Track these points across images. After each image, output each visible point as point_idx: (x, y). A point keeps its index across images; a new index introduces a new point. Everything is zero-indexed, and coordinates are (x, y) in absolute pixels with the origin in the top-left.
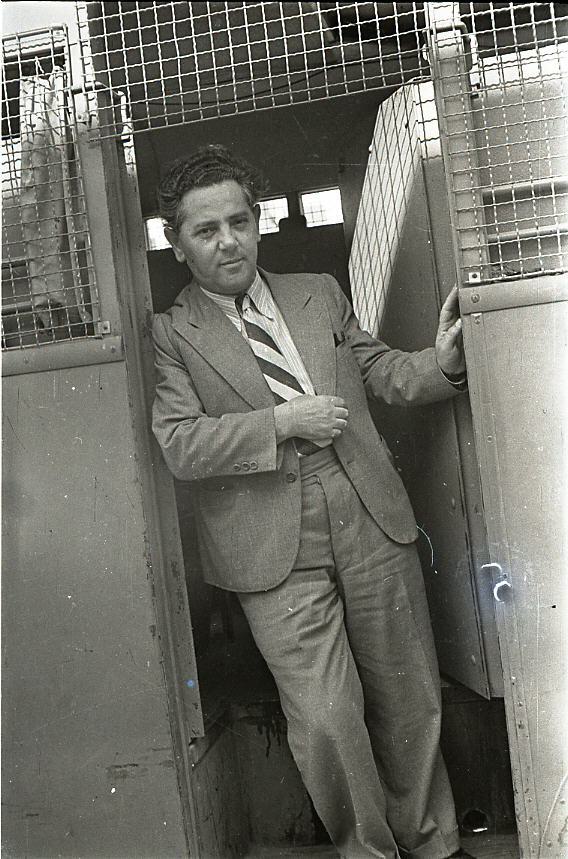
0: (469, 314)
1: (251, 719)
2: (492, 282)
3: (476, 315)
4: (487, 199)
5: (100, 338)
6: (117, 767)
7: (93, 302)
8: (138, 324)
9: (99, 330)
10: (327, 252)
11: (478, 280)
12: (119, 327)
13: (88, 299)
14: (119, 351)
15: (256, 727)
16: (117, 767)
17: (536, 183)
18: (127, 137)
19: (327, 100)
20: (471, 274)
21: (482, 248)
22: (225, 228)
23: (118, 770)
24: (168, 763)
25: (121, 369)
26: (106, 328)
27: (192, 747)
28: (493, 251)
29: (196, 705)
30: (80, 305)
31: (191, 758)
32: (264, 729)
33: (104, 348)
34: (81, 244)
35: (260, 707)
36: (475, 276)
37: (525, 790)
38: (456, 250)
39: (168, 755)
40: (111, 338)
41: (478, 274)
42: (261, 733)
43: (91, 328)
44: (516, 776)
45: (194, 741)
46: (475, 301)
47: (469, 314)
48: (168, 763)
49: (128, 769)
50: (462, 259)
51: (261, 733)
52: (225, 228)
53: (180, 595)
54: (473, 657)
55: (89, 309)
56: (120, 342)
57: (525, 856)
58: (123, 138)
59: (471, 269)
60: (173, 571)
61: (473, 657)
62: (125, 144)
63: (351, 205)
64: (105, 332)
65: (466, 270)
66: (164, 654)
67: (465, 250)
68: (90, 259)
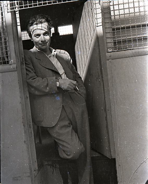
0: (108, 60)
1: (49, 165)
2: (114, 52)
3: (110, 60)
4: (113, 30)
5: (10, 65)
6: (15, 177)
7: (8, 55)
8: (20, 62)
9: (10, 63)
10: (68, 43)
11: (111, 51)
12: (15, 62)
13: (7, 54)
14: (15, 68)
15: (50, 167)
16: (15, 177)
17: (126, 25)
18: (17, 10)
19: (37, 7)
20: (109, 49)
21: (112, 42)
22: (42, 35)
23: (15, 178)
24: (29, 176)
25: (15, 74)
26: (12, 62)
27: (35, 172)
28: (115, 43)
29: (35, 161)
30: (5, 56)
31: (34, 175)
32: (52, 167)
33: (11, 67)
34: (5, 39)
35: (51, 161)
36: (110, 50)
37: (120, 181)
38: (105, 43)
39: (29, 174)
40: (13, 65)
41: (111, 49)
42: (51, 168)
43: (8, 62)
44: (118, 179)
45: (35, 170)
46: (110, 56)
47: (108, 60)
48: (29, 176)
49: (18, 178)
50: (107, 45)
51: (51, 168)
52: (42, 35)
53: (31, 133)
54: (107, 148)
55: (7, 57)
56: (16, 66)
57: (119, 183)
58: (16, 11)
59: (110, 48)
60: (30, 127)
61: (107, 148)
62: (16, 12)
63: (76, 29)
64: (12, 63)
65: (108, 48)
66: (28, 148)
67: (107, 33)
68: (7, 43)
